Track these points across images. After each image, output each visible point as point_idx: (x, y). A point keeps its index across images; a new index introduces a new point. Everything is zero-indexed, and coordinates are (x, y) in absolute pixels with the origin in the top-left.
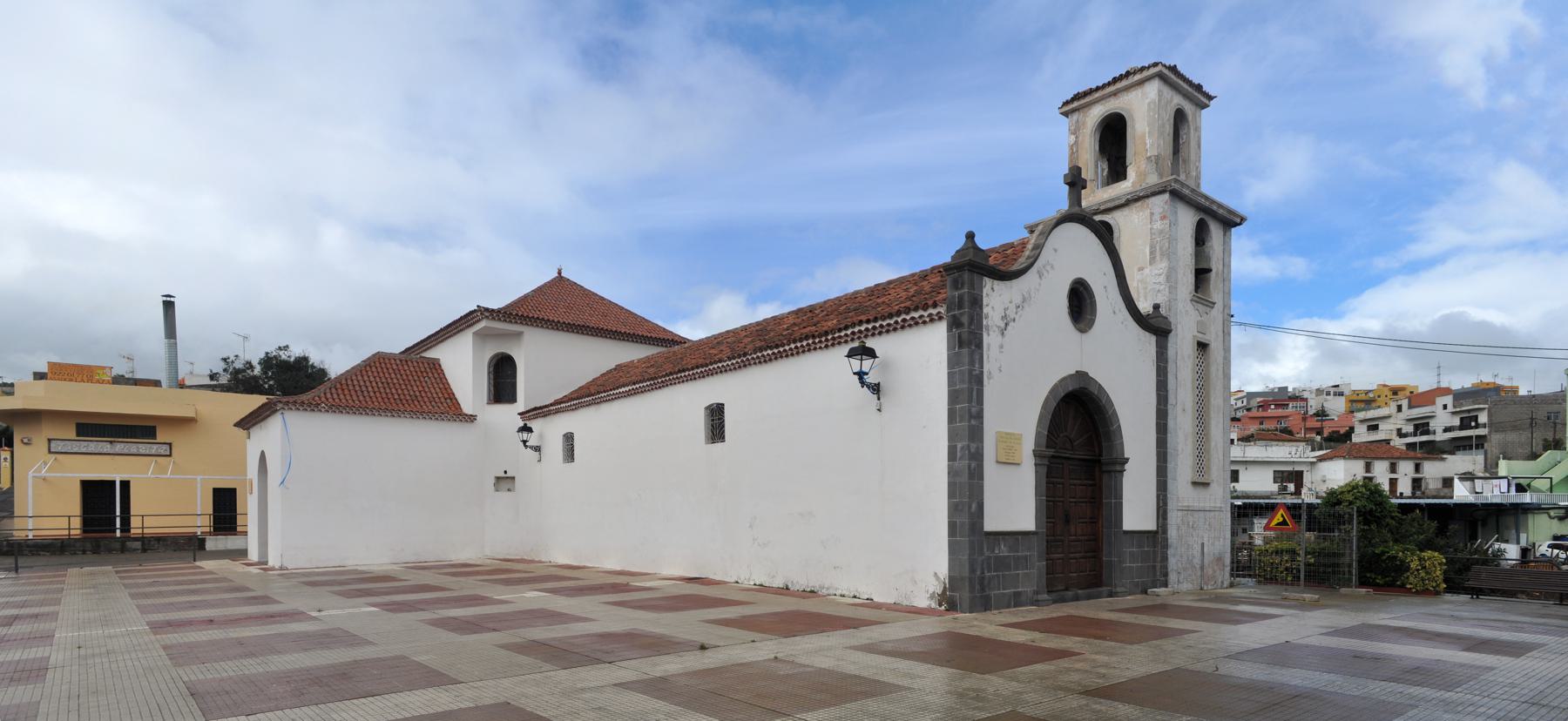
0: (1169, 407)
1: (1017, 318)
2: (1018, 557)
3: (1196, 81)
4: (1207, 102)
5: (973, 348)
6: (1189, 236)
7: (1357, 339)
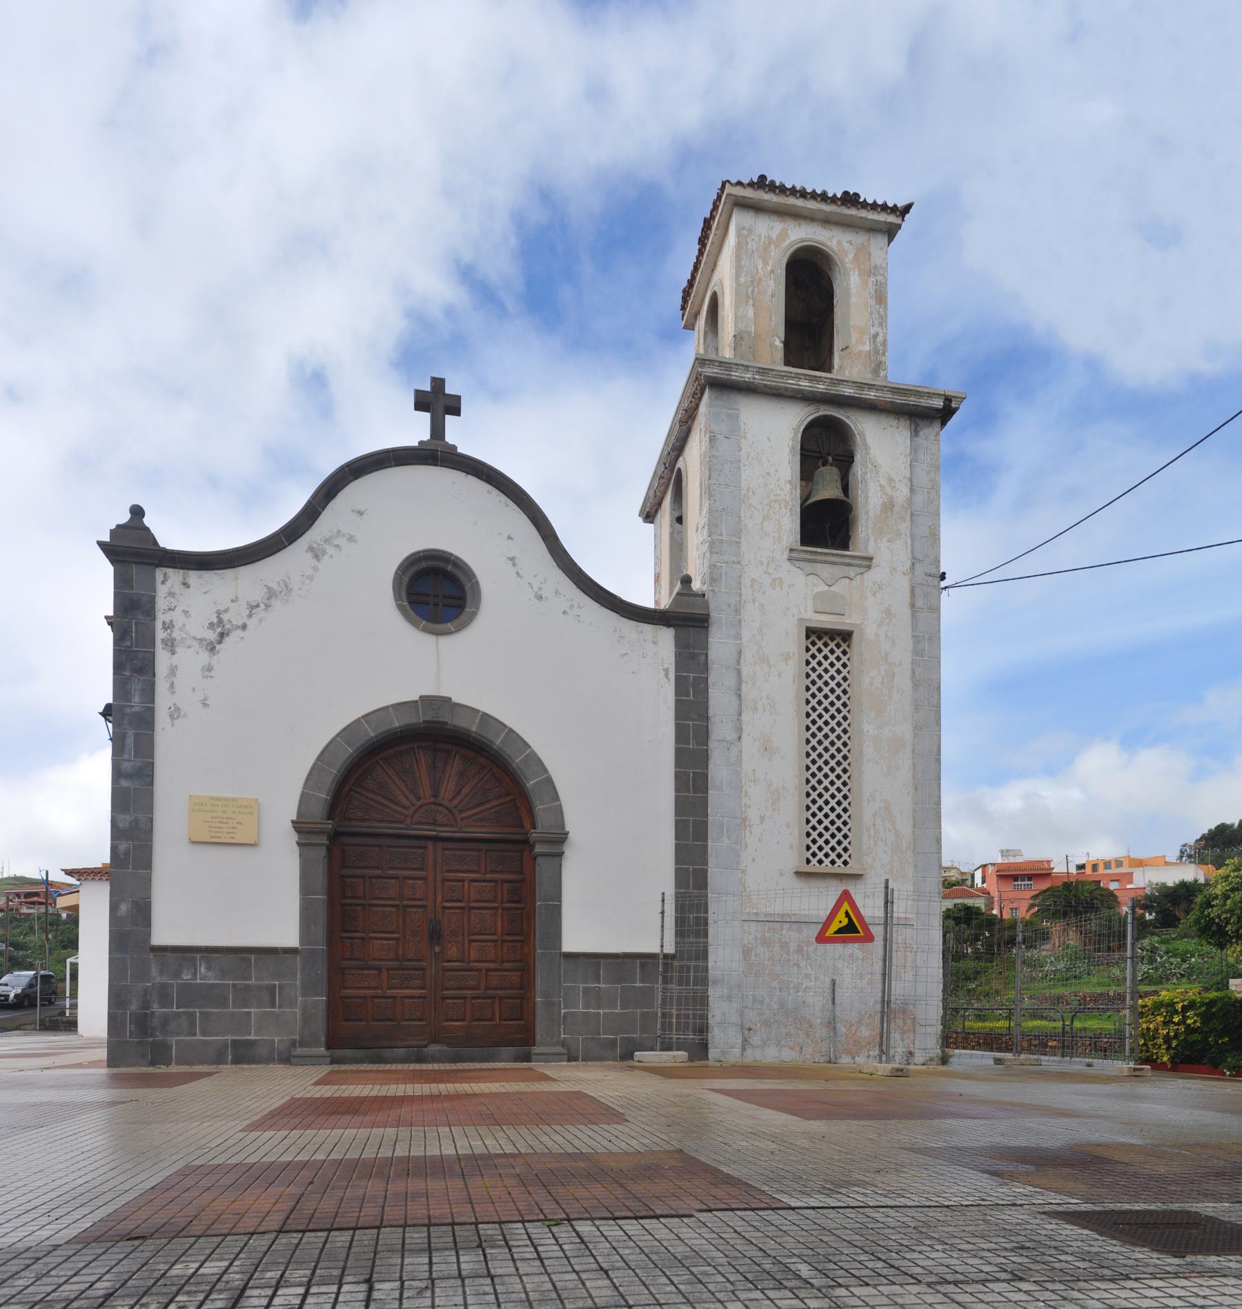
0: (712, 745)
1: (251, 623)
2: (248, 988)
3: (836, 190)
4: (898, 221)
5: (128, 673)
6: (787, 450)
7: (895, 390)
